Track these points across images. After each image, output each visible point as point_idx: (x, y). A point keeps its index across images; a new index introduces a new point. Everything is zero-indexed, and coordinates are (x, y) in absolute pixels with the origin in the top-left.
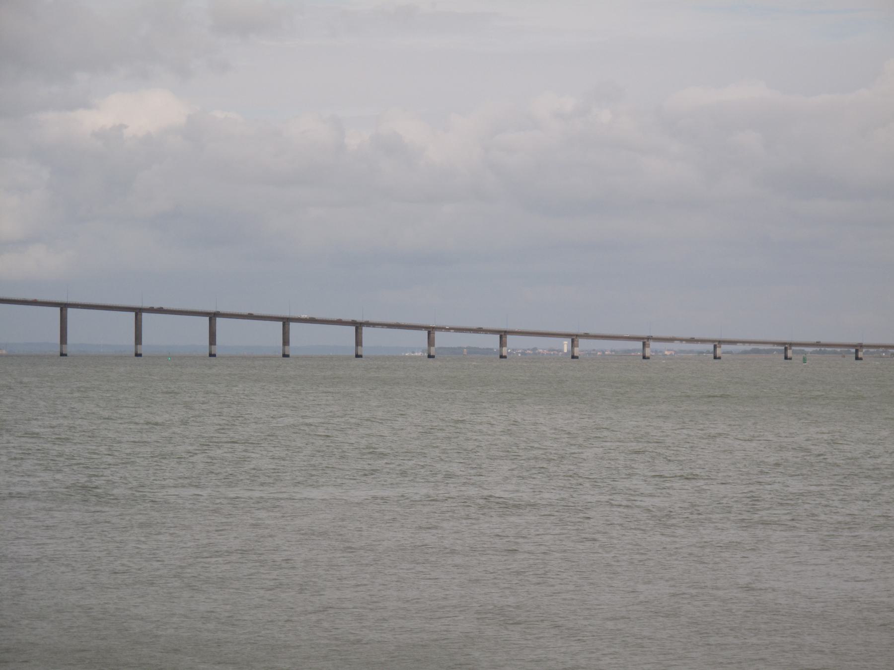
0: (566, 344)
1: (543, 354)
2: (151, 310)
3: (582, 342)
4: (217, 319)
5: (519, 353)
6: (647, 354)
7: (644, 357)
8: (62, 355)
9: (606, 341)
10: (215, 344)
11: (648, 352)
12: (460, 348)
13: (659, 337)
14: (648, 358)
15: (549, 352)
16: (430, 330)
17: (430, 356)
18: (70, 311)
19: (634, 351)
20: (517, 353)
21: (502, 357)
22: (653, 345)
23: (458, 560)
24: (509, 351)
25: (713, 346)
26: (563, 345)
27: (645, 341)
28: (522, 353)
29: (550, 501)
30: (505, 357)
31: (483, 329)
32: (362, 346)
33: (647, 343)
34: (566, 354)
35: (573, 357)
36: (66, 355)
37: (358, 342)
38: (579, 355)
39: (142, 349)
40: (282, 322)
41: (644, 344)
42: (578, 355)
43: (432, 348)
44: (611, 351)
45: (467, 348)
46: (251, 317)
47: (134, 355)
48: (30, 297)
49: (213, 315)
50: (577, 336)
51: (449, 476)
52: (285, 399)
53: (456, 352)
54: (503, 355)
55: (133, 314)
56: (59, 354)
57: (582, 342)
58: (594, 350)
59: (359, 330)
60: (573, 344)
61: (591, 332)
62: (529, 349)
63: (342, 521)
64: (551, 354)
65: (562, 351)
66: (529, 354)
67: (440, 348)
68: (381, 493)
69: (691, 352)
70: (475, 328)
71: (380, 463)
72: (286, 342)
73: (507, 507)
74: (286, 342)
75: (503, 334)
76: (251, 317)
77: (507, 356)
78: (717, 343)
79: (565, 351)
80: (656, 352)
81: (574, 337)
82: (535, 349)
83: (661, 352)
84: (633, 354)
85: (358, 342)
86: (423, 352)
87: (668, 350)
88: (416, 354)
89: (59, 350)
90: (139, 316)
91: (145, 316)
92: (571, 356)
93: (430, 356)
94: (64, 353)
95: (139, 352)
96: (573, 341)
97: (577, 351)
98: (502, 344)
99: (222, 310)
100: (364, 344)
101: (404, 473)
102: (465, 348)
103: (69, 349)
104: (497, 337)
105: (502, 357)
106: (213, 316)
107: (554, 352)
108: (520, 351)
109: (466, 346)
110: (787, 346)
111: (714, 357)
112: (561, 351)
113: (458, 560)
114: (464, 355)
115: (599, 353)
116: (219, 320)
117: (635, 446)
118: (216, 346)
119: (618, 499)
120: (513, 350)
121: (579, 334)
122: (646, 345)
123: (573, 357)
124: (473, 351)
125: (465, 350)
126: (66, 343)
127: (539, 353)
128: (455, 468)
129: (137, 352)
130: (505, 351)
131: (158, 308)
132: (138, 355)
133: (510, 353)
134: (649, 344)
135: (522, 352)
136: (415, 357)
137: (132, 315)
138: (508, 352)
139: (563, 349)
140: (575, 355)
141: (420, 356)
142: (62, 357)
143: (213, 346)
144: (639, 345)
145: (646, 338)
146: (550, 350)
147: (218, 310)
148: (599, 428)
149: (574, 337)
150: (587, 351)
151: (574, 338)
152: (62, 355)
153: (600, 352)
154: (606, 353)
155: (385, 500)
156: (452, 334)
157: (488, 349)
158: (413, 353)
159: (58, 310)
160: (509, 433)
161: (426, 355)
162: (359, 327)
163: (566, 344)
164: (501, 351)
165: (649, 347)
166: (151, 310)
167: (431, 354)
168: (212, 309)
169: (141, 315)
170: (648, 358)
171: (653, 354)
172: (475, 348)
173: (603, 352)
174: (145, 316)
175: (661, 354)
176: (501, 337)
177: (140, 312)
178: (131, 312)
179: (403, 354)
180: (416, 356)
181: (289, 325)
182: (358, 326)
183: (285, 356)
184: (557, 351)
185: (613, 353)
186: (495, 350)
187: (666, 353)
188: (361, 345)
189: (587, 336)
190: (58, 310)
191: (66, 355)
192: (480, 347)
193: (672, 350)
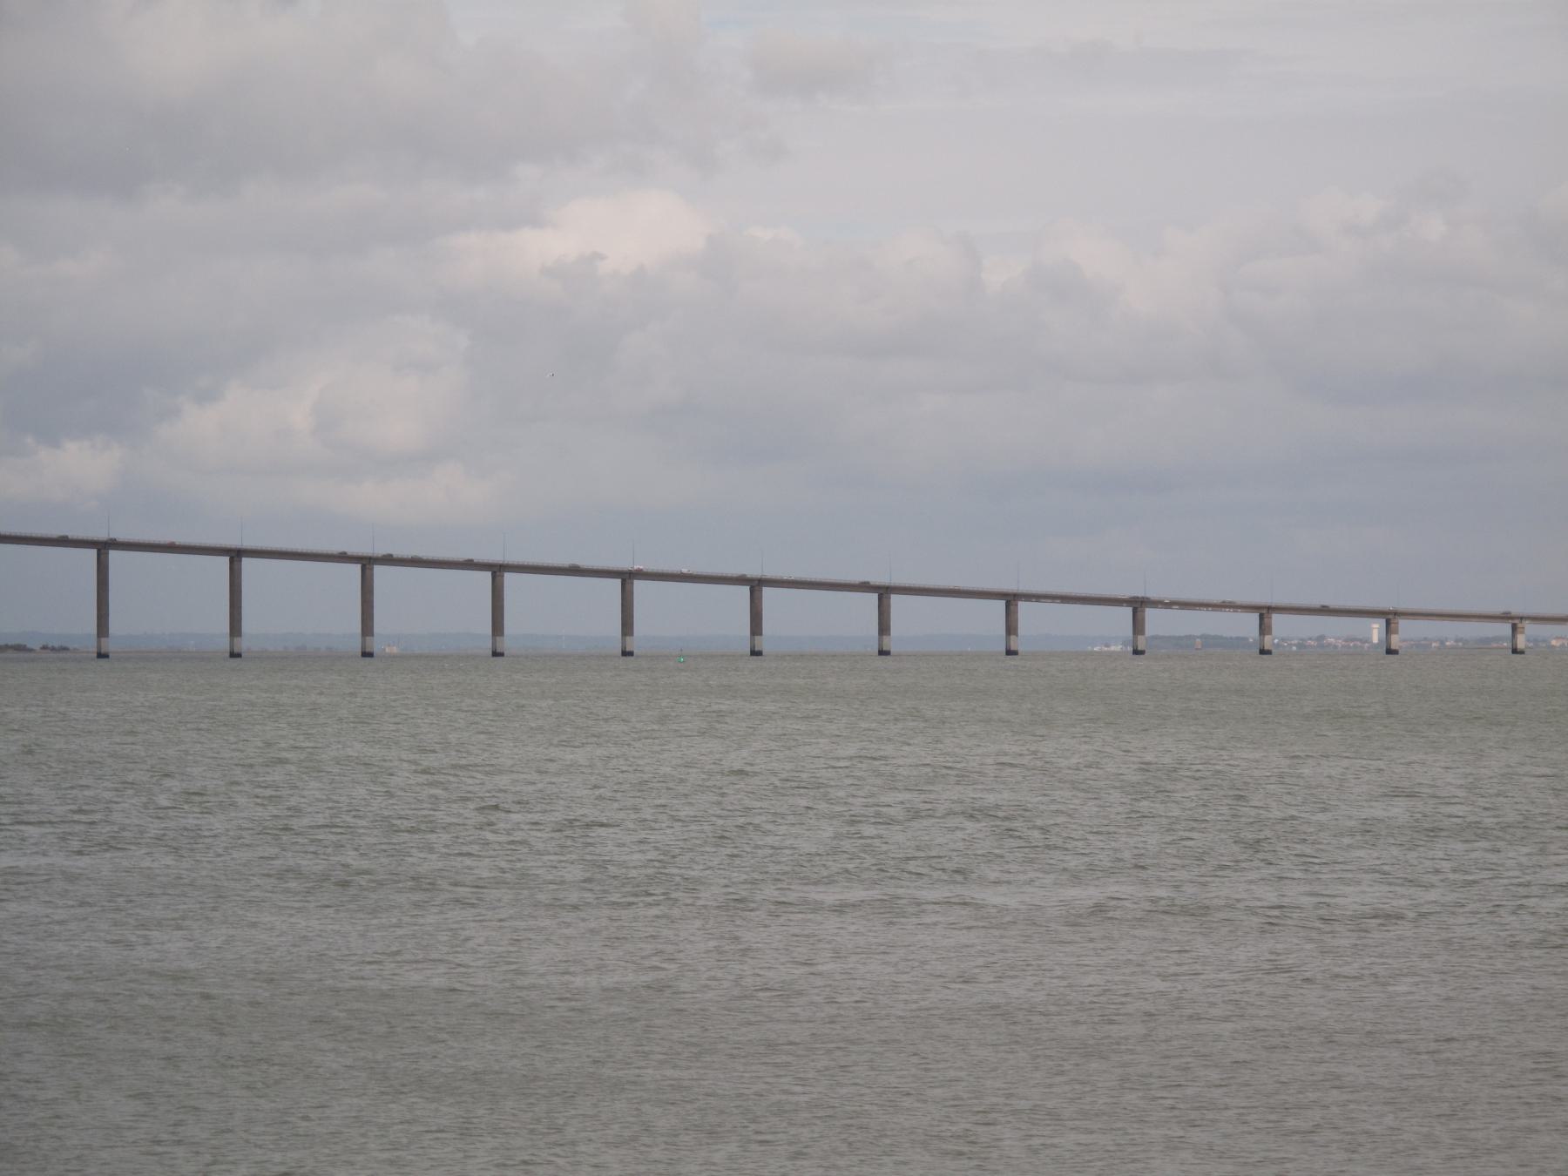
0: (1376, 629)
1: (1336, 647)
2: (389, 560)
4: (1020, 603)
5: (1295, 645)
6: (1521, 644)
7: (1515, 651)
8: (496, 654)
9: (1490, 624)
10: (632, 634)
11: (1521, 642)
12: (1189, 637)
13: (941, 587)
14: (1522, 652)
15: (1346, 644)
16: (1009, 599)
17: (1136, 652)
18: (638, 585)
19: (1497, 639)
20: (1291, 645)
21: (1263, 652)
22: (1530, 629)
24: (1276, 641)
25: (1510, 625)
26: (1371, 629)
28: (1300, 646)
29: (337, 1140)
30: (1269, 652)
31: (395, 556)
32: (1017, 636)
33: (1519, 625)
34: (1376, 646)
35: (1390, 651)
36: (502, 655)
37: (1011, 629)
38: (1400, 647)
39: (634, 644)
40: (748, 587)
41: (1514, 628)
42: (1397, 648)
43: (1139, 637)
44: (1457, 641)
45: (1201, 637)
46: (574, 571)
47: (360, 654)
49: (757, 582)
50: (1396, 614)
52: (735, 760)
53: (1182, 645)
54: (1266, 648)
55: (875, 597)
56: (748, 651)
57: (1403, 624)
58: (1425, 639)
59: (1012, 607)
60: (1389, 629)
61: (398, 552)
62: (1310, 639)
63: (741, 964)
64: (1349, 647)
65: (1368, 640)
66: (1310, 646)
67: (1155, 638)
70: (335, 553)
72: (884, 628)
74: (884, 628)
75: (1265, 613)
76: (574, 571)
77: (1273, 651)
79: (1375, 640)
80: (1536, 641)
81: (1390, 617)
82: (1321, 638)
83: (1544, 641)
84: (1495, 645)
85: (1011, 629)
86: (1125, 644)
87: (1557, 638)
88: (1113, 648)
89: (490, 645)
90: (368, 571)
91: (509, 578)
92: (1385, 649)
93: (1136, 652)
94: (498, 651)
95: (1013, 648)
96: (1388, 623)
97: (1395, 641)
98: (1264, 629)
100: (1021, 631)
102: (1198, 637)
103: (507, 643)
105: (1263, 652)
106: (627, 578)
107: (1356, 643)
108: (1296, 642)
109: (1199, 634)
111: (1134, 650)
112: (1366, 642)
114: (1197, 649)
115: (1434, 645)
116: (767, 592)
118: (763, 637)
120: (1283, 640)
121: (1273, 605)
122: (1519, 630)
123: (1390, 651)
124: (1210, 641)
125: (1198, 640)
126: (502, 634)
127: (1329, 644)
129: (1390, 646)
130: (1268, 642)
131: (384, 556)
132: (367, 654)
133: (1278, 645)
134: (1523, 628)
135: (1299, 643)
136: (1111, 655)
137: (873, 598)
138: (1274, 644)
139: (1372, 638)
140: (1393, 647)
141: (1119, 652)
142: (495, 658)
143: (757, 638)
144: (1505, 629)
145: (1518, 618)
146: (1348, 640)
147: (1148, 595)
149: (1390, 617)
150: (1412, 640)
151: (1390, 618)
152: (496, 654)
153: (1436, 641)
154: (1448, 643)
156: (1175, 613)
157: (1237, 638)
158: (1107, 646)
159: (357, 568)
161: (1130, 649)
162: (1139, 609)
163: (1376, 629)
164: (1262, 641)
165: (1396, 632)
166: (389, 560)
167: (1139, 648)
168: (102, 535)
169: (372, 569)
170: (1522, 652)
171: (1531, 645)
172: (1215, 637)
173: (1442, 643)
174: (896, 600)
175: (1544, 645)
176: (1261, 617)
177: (758, 585)
178: (85, 548)
179: (1089, 648)
180: (1114, 652)
181: (632, 583)
182: (1011, 600)
183: (755, 653)
184: (1361, 640)
185: (1460, 644)
186: (1251, 640)
187: (1554, 642)
188: (1016, 634)
190: (225, 560)
191: (502, 655)
192: (1224, 635)
193: (1563, 638)
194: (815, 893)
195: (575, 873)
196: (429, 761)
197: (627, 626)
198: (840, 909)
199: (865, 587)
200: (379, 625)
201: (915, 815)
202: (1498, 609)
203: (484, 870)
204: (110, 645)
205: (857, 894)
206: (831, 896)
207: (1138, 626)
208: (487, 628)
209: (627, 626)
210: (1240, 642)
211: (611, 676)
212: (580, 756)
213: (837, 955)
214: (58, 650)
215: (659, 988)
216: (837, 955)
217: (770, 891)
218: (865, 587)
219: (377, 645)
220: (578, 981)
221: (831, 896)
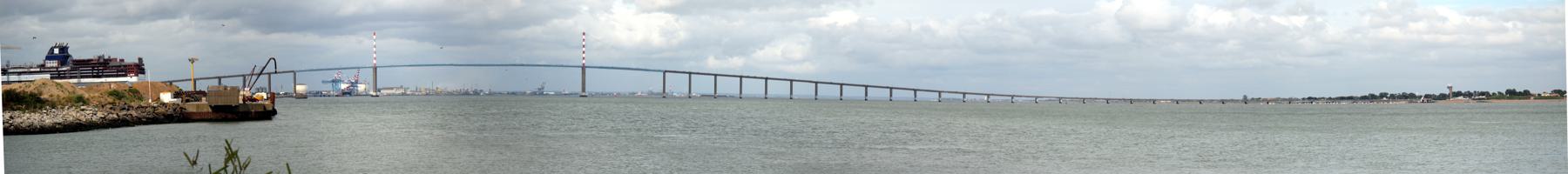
3: (991, 97)
18: (692, 75)
23: (949, 170)
27: (1013, 97)
39: (843, 98)
48: (611, 66)
51: (945, 142)
52: (862, 120)
53: (994, 101)
57: (991, 97)
60: (988, 97)
68: (921, 147)
69: (107, 76)
71: (923, 137)
72: (891, 96)
73: (965, 152)
74: (891, 96)
75: (964, 94)
78: (1037, 97)
91: (718, 77)
99: (744, 75)
101: (930, 141)
104: (937, 94)
106: (842, 85)
110: (1060, 98)
113: (949, 170)
117: (1008, 132)
119: (1003, 150)
128: (948, 139)
137: (839, 86)
148: (997, 126)
151: (988, 95)
155: (924, 149)
160: (966, 127)
163: (986, 98)
174: (718, 77)
182: (915, 90)
189: (993, 95)
194: (877, 146)
195: (831, 142)
196: (803, 119)
197: (841, 94)
198: (881, 149)
199: (888, 87)
200: (794, 93)
201: (896, 132)
202: (687, 71)
203: (813, 141)
204: (742, 96)
205: (885, 146)
206: (880, 147)
207: (940, 96)
208: (814, 93)
209: (841, 94)
210: (959, 100)
211: (1303, 167)
212: (831, 119)
213: (881, 158)
214: (732, 97)
215: (846, 164)
216: (881, 158)
217: (868, 146)
218: (888, 87)
219: (793, 97)
220: (831, 162)
221: (880, 147)
